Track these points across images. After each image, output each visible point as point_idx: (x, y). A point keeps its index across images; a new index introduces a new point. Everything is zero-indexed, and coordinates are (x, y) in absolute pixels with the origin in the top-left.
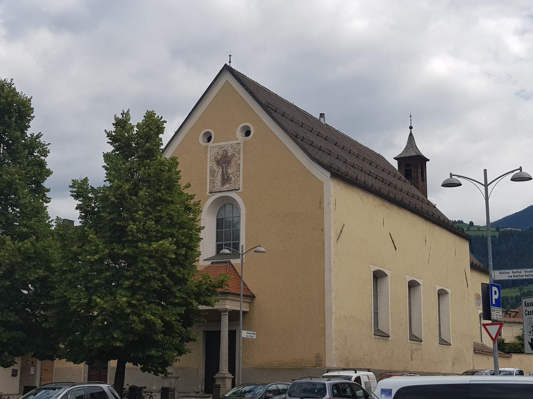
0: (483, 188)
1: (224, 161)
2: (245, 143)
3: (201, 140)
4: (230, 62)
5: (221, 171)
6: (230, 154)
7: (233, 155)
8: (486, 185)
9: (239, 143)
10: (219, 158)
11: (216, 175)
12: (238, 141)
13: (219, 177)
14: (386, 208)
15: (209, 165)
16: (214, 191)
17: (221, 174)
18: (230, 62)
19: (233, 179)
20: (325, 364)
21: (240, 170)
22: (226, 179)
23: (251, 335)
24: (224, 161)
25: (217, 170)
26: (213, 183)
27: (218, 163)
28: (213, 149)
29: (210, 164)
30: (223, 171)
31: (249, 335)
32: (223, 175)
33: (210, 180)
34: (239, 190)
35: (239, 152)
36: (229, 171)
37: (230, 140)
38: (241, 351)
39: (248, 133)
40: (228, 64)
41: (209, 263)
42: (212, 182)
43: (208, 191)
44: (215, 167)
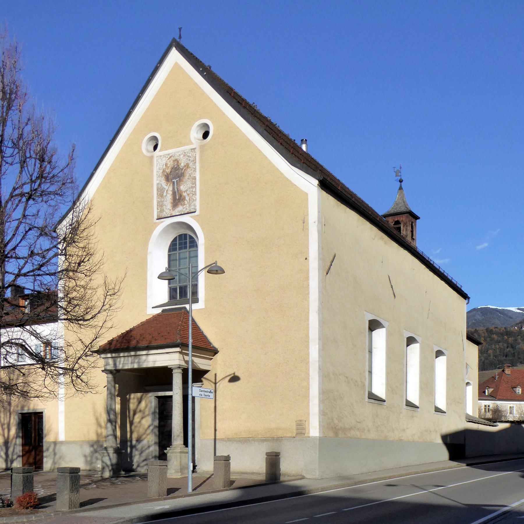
0: (213, 385)
1: (175, 174)
2: (202, 147)
3: (146, 147)
4: (180, 37)
5: (171, 188)
6: (182, 165)
7: (187, 166)
8: (215, 383)
9: (194, 149)
10: (168, 171)
11: (165, 194)
12: (192, 147)
13: (169, 198)
14: (386, 243)
15: (155, 181)
16: (163, 216)
17: (171, 193)
18: (180, 37)
19: (187, 198)
20: (309, 433)
21: (195, 187)
22: (178, 199)
23: (206, 394)
24: (175, 174)
25: (166, 188)
26: (162, 206)
27: (168, 178)
28: (161, 159)
29: (157, 180)
30: (174, 189)
31: (203, 393)
32: (174, 193)
33: (158, 202)
34: (195, 212)
35: (194, 161)
36: (182, 188)
37: (181, 144)
38: (33, 435)
39: (206, 135)
40: (178, 40)
41: (159, 311)
42: (160, 205)
43: (156, 217)
44: (163, 183)
